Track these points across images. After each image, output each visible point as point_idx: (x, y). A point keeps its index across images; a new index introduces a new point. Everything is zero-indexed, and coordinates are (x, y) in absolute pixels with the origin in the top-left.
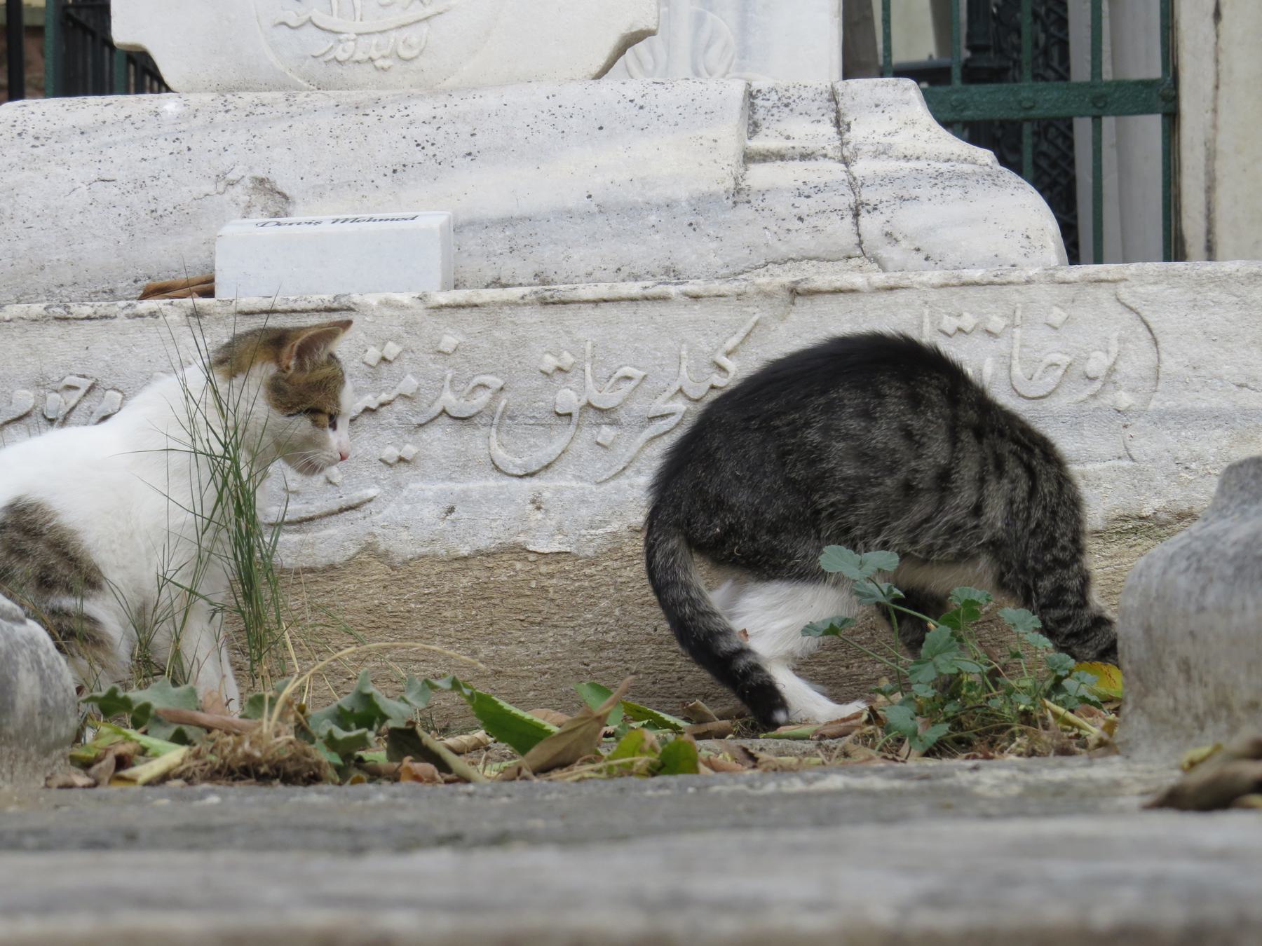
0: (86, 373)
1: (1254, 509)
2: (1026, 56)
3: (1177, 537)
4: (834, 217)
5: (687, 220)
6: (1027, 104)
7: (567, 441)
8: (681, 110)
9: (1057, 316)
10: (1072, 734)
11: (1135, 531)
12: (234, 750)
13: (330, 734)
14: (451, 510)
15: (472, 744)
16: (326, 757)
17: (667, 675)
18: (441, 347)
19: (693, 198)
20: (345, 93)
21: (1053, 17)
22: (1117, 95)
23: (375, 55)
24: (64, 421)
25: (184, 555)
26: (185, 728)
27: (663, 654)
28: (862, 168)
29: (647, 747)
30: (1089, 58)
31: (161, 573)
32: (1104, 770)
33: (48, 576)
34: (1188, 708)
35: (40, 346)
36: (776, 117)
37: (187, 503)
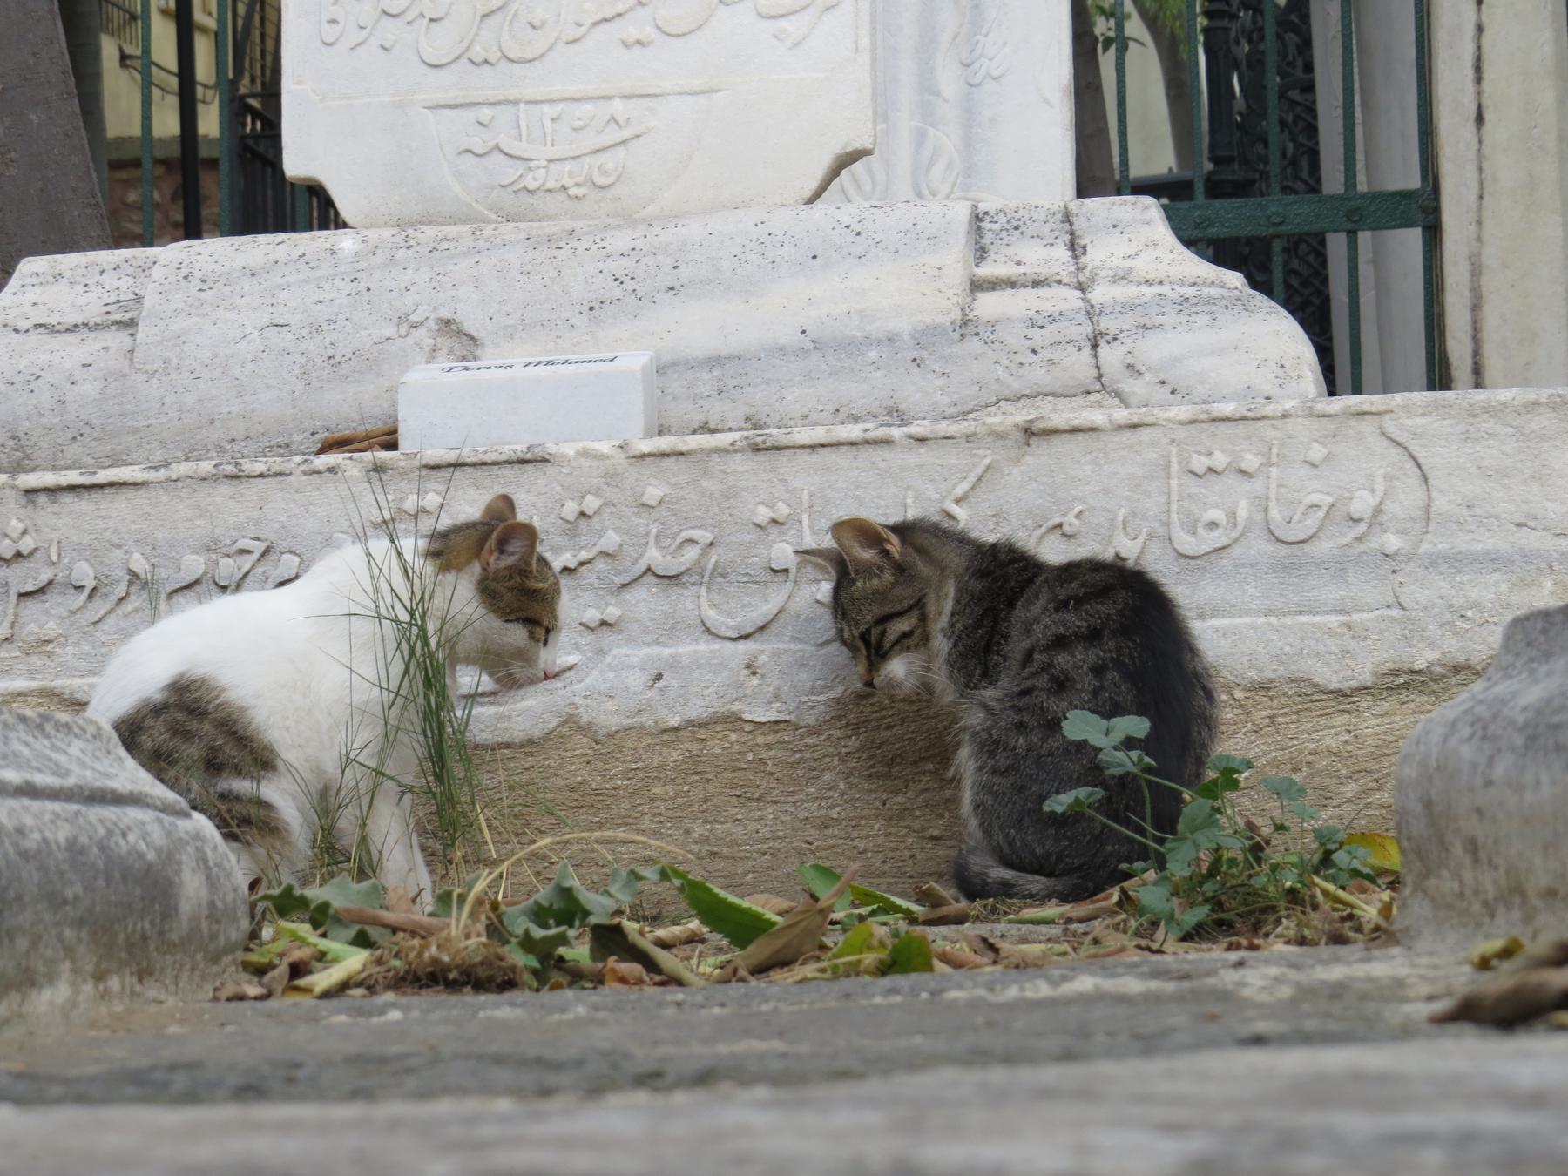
0: (260, 536)
1: (1544, 669)
2: (1274, 167)
3: (1457, 700)
4: (1071, 349)
5: (910, 355)
6: (1277, 220)
7: (784, 599)
8: (901, 235)
9: (1317, 452)
10: (1345, 913)
11: (1407, 686)
12: (420, 954)
13: (527, 932)
14: (659, 677)
15: (685, 936)
16: (521, 959)
17: (898, 853)
18: (645, 500)
19: (916, 331)
20: (536, 225)
21: (1301, 124)
22: (1372, 209)
23: (568, 182)
24: (238, 587)
25: (366, 737)
26: (369, 929)
27: (894, 830)
28: (1099, 294)
29: (875, 942)
30: (1342, 168)
31: (344, 752)
32: (1385, 966)
33: (216, 758)
34: (1476, 892)
35: (210, 508)
36: (1005, 241)
37: (372, 676)
